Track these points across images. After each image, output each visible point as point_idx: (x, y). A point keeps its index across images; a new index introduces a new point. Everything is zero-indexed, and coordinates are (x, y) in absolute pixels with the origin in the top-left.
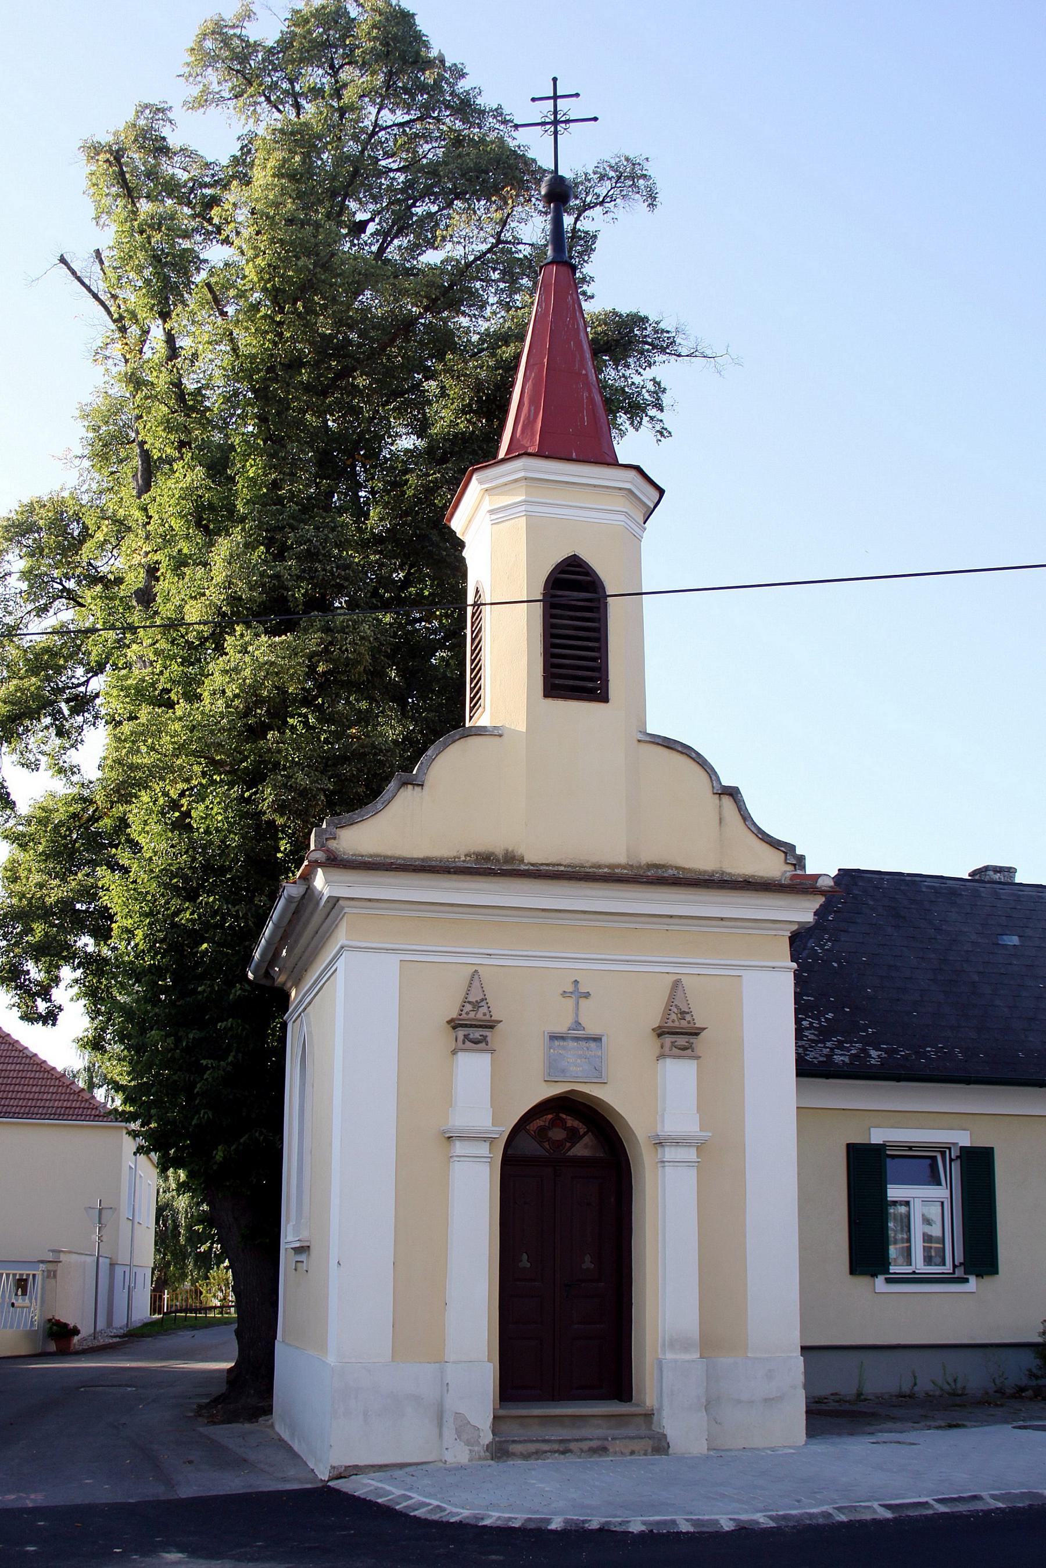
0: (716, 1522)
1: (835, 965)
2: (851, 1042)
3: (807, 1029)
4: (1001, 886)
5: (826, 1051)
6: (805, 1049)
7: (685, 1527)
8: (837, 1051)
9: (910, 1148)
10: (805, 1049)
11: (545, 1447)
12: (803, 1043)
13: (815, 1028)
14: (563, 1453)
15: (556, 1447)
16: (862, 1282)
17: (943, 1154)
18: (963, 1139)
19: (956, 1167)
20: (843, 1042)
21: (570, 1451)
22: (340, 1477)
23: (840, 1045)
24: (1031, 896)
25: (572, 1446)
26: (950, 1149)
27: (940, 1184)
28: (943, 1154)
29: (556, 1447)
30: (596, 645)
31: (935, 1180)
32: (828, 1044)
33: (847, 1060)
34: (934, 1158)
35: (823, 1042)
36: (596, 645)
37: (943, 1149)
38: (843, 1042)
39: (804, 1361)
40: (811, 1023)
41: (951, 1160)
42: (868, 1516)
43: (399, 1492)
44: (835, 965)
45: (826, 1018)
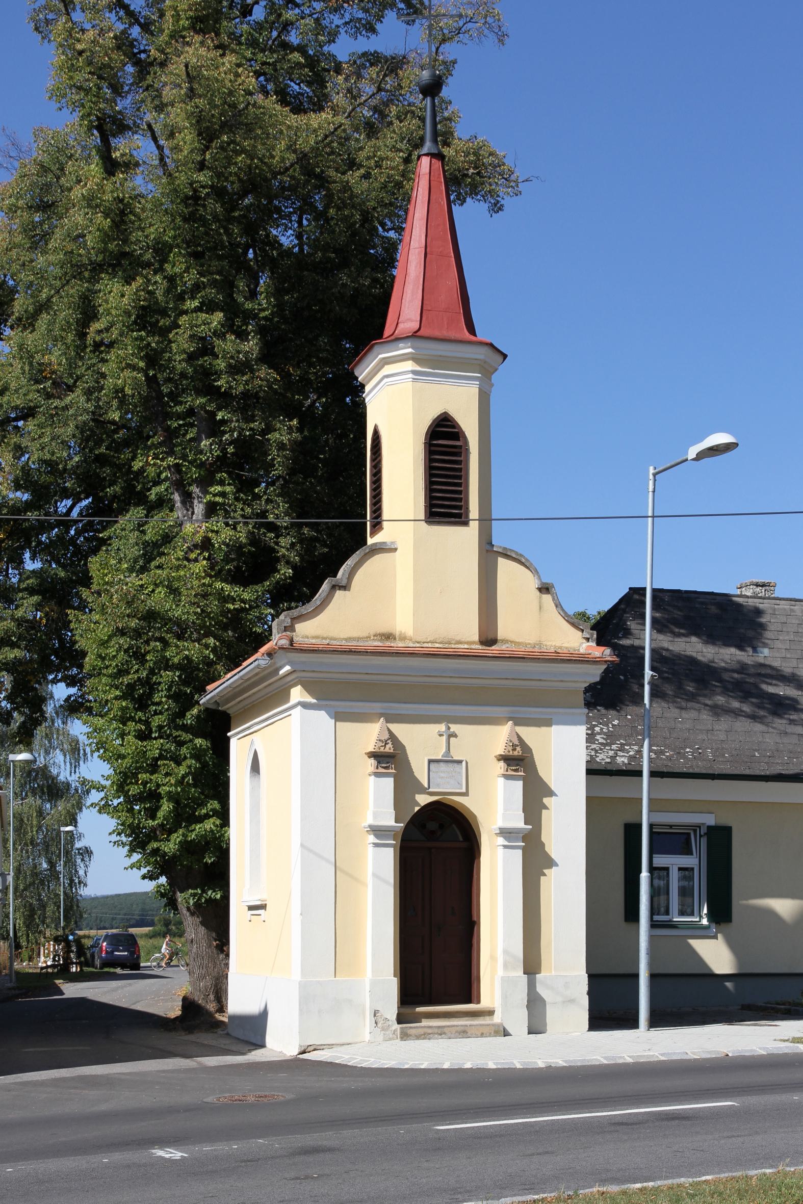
0: (536, 1063)
1: (622, 677)
2: (630, 745)
3: (599, 734)
4: (761, 601)
5: (611, 753)
6: (596, 751)
7: (519, 1066)
8: (620, 753)
9: (671, 826)
10: (596, 751)
11: (430, 1031)
12: (594, 746)
13: (605, 734)
14: (441, 1034)
15: (436, 1031)
16: (724, 821)
17: (695, 831)
18: (710, 820)
19: (704, 841)
20: (625, 745)
21: (445, 1033)
22: (304, 1052)
23: (622, 749)
24: (785, 609)
25: (445, 1030)
26: (700, 827)
27: (692, 854)
28: (695, 831)
29: (436, 1031)
30: (433, 448)
31: (688, 851)
32: (614, 747)
33: (626, 761)
34: (689, 834)
35: (610, 745)
36: (433, 448)
37: (696, 827)
38: (625, 745)
39: (146, 893)
40: (602, 729)
41: (701, 836)
42: (621, 1061)
43: (347, 1057)
44: (622, 677)
45: (613, 725)
